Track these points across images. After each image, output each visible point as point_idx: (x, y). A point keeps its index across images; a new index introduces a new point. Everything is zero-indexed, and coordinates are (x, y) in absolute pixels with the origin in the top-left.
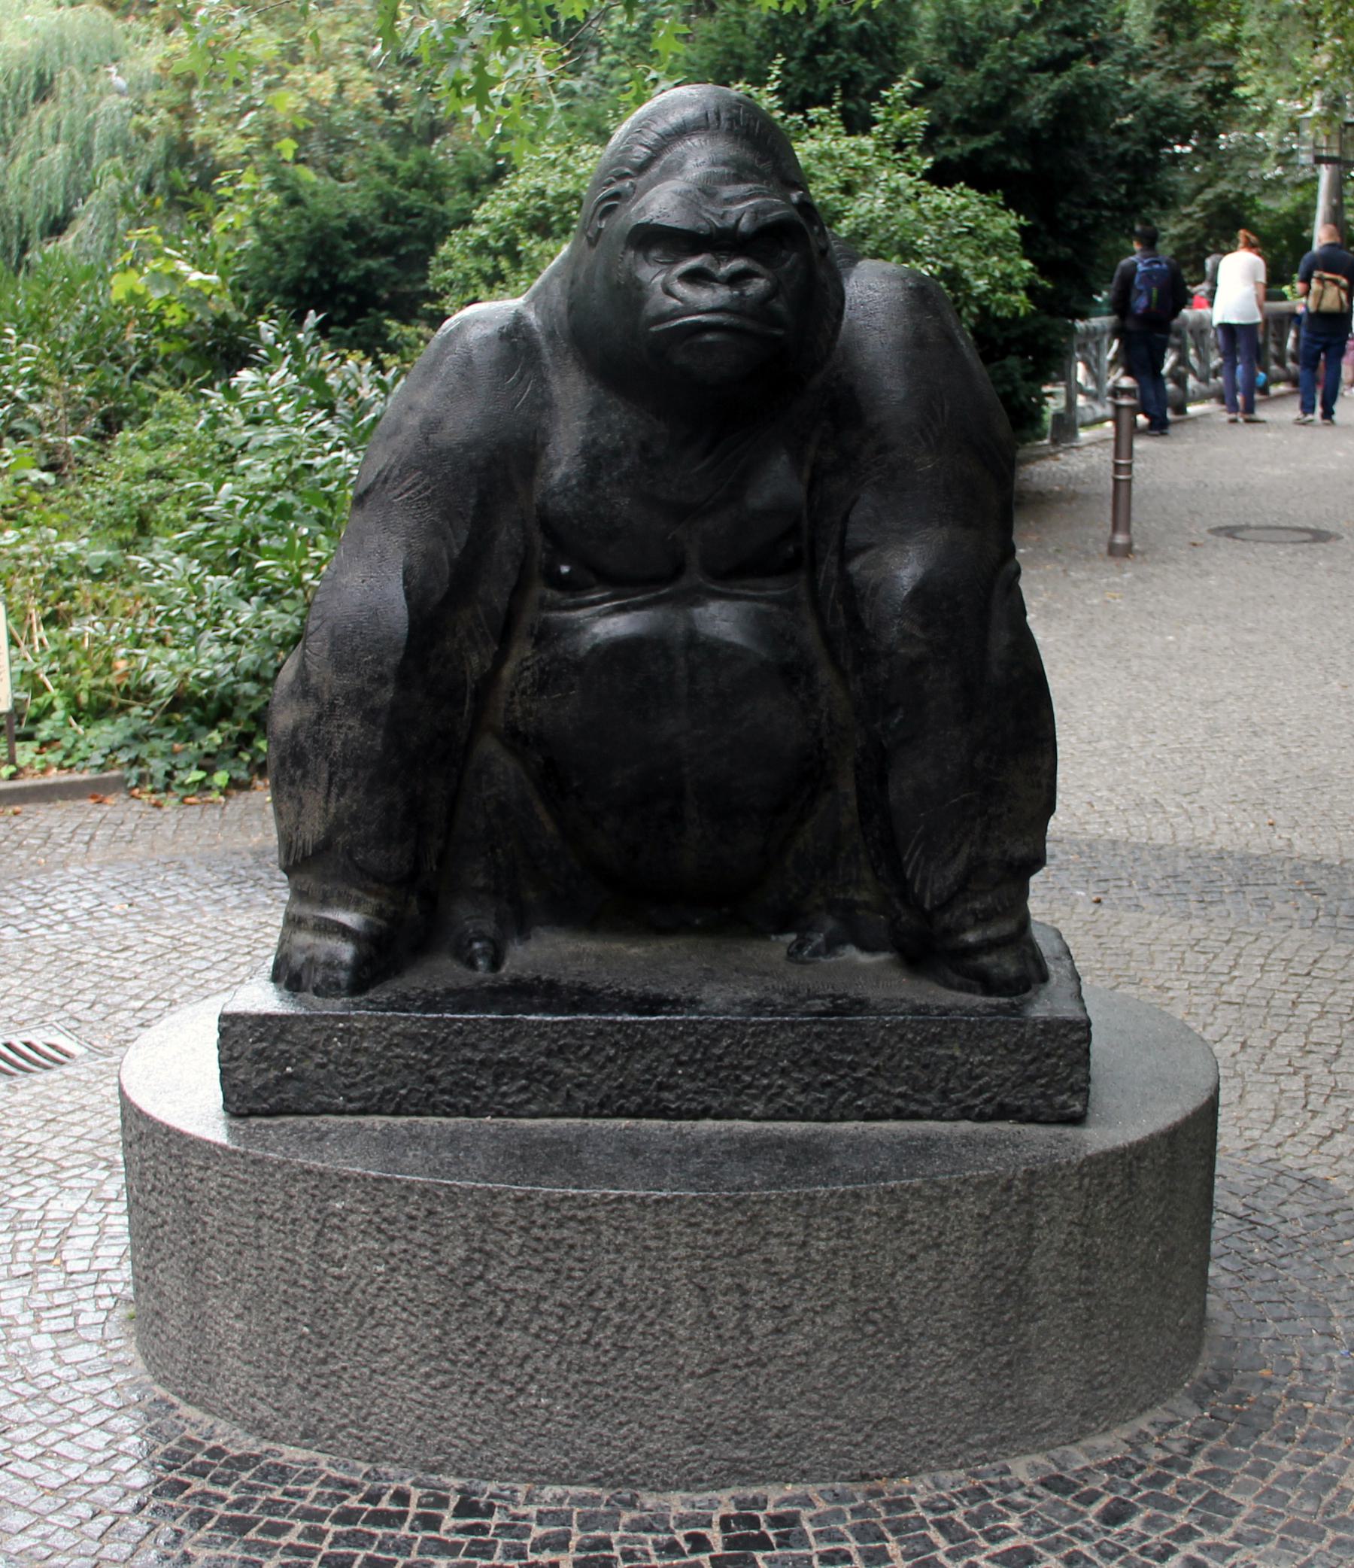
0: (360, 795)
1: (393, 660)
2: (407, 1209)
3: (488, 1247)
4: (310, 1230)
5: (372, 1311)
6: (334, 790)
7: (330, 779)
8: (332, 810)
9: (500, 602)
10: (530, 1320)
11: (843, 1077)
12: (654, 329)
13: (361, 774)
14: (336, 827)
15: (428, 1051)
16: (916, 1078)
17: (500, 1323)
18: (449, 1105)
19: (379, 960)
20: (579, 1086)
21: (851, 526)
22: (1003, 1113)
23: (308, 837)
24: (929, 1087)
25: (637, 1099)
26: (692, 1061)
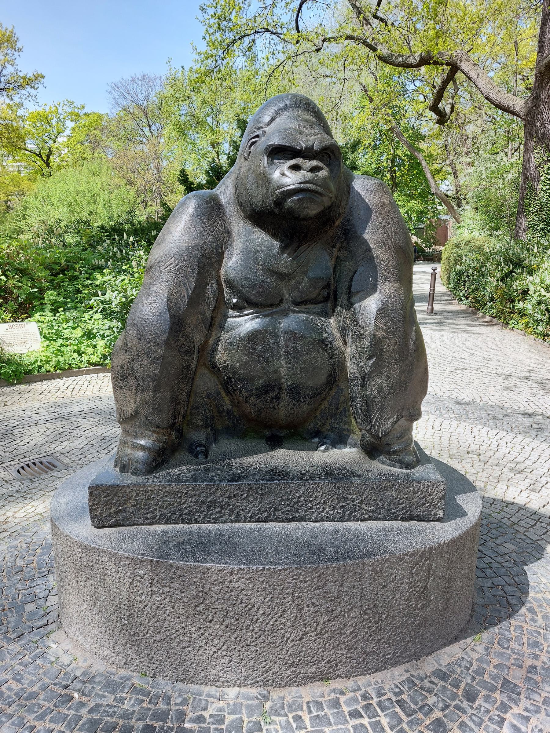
0: (150, 393)
1: (164, 337)
2: (170, 575)
3: (205, 590)
4: (128, 581)
5: (154, 616)
6: (139, 391)
7: (137, 387)
8: (138, 400)
9: (208, 314)
10: (223, 621)
11: (348, 504)
12: (277, 192)
13: (151, 385)
14: (141, 406)
15: (180, 498)
16: (377, 504)
17: (210, 622)
18: (188, 519)
19: (159, 460)
20: (242, 510)
21: (353, 283)
22: (411, 518)
23: (128, 410)
24: (383, 508)
25: (265, 514)
26: (288, 499)
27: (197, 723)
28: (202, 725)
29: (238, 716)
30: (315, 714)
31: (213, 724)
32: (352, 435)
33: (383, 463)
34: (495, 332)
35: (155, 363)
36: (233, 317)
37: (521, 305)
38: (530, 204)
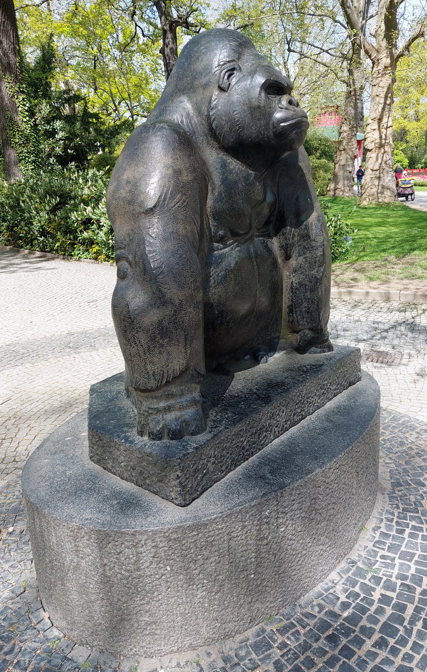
12: (282, 124)
27: (401, 580)
28: (352, 606)
29: (359, 584)
30: (386, 548)
31: (356, 599)
32: (281, 340)
33: (315, 353)
34: (59, 267)
35: (198, 308)
36: (218, 250)
37: (85, 235)
38: (14, 135)
